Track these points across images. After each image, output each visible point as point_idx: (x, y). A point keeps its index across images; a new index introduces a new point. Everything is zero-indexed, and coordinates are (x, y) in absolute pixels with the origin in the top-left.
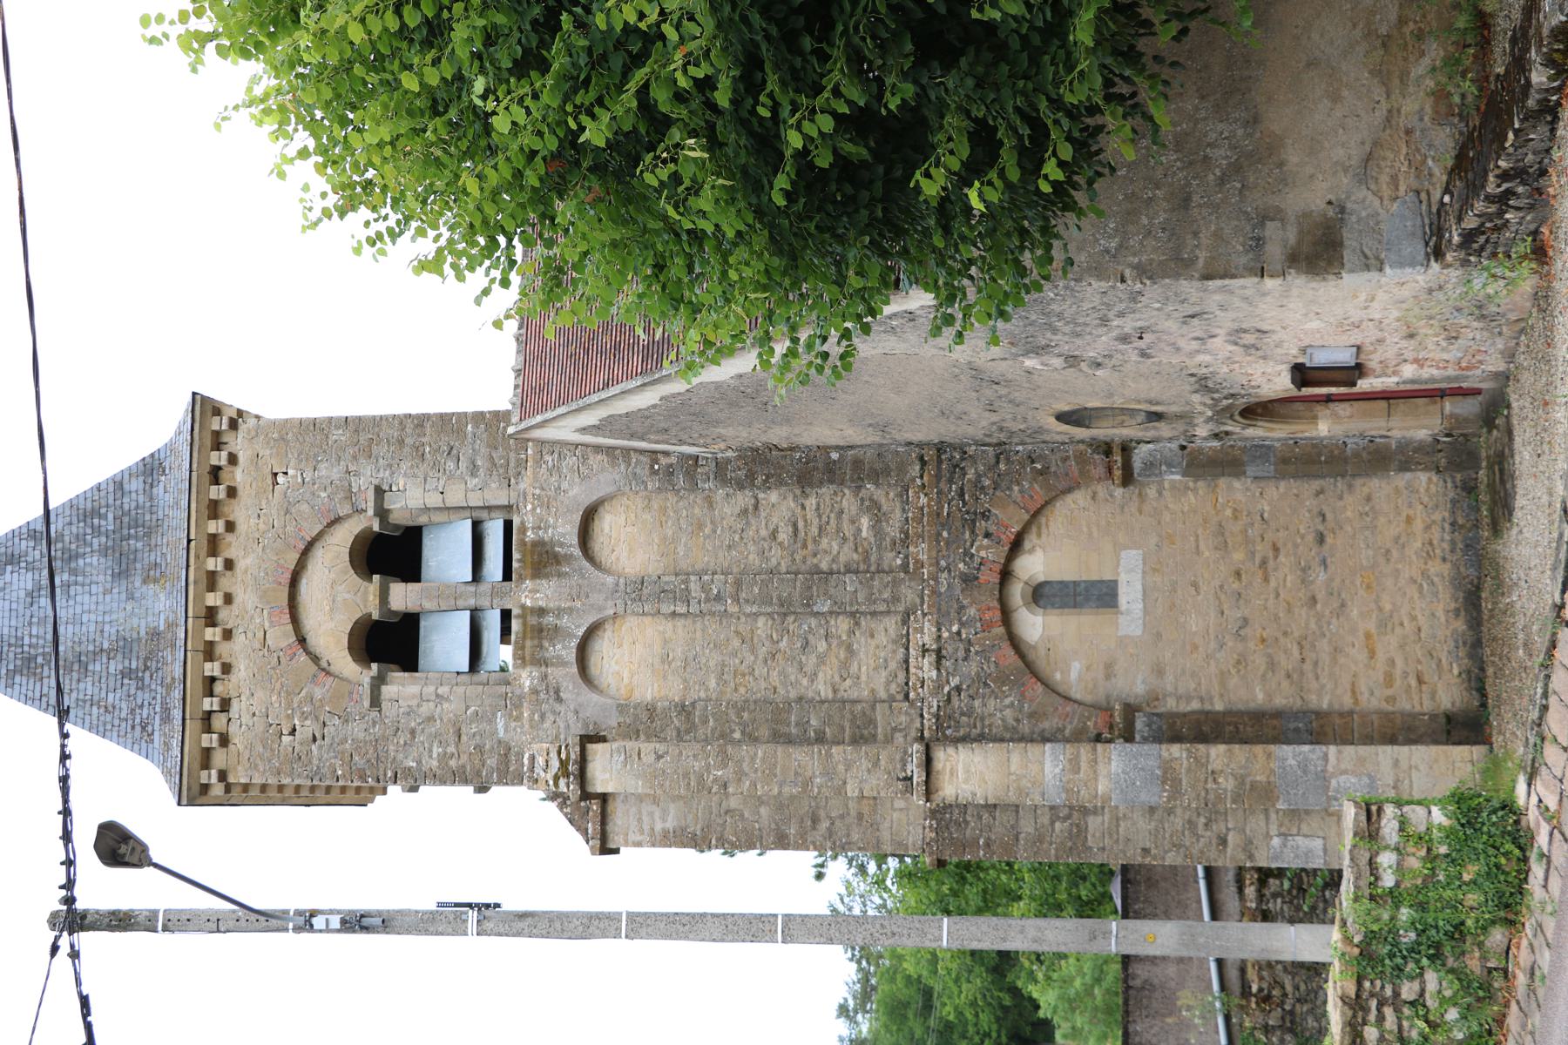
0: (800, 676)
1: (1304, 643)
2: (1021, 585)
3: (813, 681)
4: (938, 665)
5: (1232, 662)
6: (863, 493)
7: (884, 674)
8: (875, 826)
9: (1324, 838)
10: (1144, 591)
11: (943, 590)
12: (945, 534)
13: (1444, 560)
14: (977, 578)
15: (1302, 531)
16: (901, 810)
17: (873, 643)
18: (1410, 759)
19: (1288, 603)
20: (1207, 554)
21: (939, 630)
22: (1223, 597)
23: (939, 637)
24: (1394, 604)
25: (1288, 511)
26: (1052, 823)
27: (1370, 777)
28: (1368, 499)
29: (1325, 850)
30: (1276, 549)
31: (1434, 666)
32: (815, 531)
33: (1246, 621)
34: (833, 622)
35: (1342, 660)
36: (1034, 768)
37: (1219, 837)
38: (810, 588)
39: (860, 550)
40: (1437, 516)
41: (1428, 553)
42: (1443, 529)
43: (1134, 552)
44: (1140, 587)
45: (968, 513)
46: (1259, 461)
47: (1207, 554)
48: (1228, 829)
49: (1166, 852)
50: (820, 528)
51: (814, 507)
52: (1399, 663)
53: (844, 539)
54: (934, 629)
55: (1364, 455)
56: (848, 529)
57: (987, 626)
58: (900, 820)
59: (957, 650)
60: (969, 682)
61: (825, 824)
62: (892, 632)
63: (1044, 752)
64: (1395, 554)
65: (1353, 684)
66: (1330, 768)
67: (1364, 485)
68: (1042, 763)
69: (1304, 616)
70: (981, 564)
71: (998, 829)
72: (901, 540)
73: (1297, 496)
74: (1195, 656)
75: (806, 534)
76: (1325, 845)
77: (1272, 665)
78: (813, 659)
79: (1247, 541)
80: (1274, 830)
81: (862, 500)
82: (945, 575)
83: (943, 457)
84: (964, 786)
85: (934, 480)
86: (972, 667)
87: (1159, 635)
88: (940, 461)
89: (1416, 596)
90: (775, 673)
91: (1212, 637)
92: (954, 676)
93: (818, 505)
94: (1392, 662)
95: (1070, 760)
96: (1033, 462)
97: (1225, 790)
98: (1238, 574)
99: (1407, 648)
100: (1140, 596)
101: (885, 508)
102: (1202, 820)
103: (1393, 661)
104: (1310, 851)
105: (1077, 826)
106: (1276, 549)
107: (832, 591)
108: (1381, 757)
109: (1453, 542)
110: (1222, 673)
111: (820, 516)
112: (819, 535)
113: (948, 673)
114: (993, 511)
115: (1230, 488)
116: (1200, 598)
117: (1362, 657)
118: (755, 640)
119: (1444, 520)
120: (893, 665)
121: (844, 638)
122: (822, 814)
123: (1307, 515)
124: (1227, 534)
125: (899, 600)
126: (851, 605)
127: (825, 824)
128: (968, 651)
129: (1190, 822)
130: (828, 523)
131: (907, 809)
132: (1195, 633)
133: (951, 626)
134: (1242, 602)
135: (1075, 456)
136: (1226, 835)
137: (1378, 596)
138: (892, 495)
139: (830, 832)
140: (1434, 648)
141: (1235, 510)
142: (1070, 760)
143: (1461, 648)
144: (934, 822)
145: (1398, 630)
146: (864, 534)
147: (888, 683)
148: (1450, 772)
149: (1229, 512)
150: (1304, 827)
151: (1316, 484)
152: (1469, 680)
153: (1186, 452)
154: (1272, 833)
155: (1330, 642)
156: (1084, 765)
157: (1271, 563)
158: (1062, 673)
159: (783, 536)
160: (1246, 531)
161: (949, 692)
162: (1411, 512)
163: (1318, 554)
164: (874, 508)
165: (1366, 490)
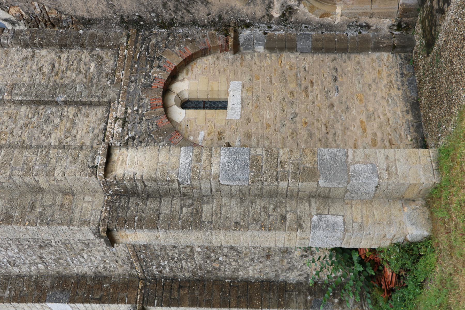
0: (41, 135)
1: (328, 125)
2: (175, 95)
3: (48, 137)
4: (123, 126)
5: (289, 133)
6: (94, 52)
7: (91, 135)
8: (71, 211)
9: (343, 216)
10: (242, 100)
11: (131, 91)
12: (136, 66)
13: (399, 89)
14: (151, 86)
15: (325, 76)
16: (89, 202)
17: (88, 120)
18: (395, 156)
19: (319, 107)
20: (276, 84)
21: (126, 109)
22: (284, 104)
23: (126, 112)
24: (374, 108)
25: (318, 67)
26: (181, 208)
27: (372, 164)
28: (359, 63)
29: (344, 223)
30: (312, 83)
31: (398, 136)
32: (64, 68)
33: (296, 115)
34: (66, 109)
35: (348, 133)
36: (173, 159)
37: (281, 215)
38: (56, 89)
39: (88, 77)
40: (394, 71)
41: (390, 86)
42: (397, 76)
43: (237, 82)
44: (239, 98)
45: (150, 57)
46: (304, 40)
47: (276, 84)
48: (286, 211)
49: (249, 224)
50: (67, 67)
51: (66, 57)
52: (379, 135)
53: (80, 72)
54: (123, 109)
55: (357, 39)
56: (82, 68)
57: (153, 108)
58: (87, 207)
59: (135, 118)
60: (140, 134)
61: (38, 210)
62: (99, 115)
63: (180, 151)
64: (373, 86)
65: (355, 144)
66: (349, 160)
67: (356, 57)
68: (179, 157)
69: (327, 112)
70: (154, 79)
71: (148, 211)
72: (111, 73)
73: (323, 61)
74: (268, 130)
75: (59, 69)
76: (344, 220)
77: (311, 135)
78: (51, 127)
79: (297, 79)
80: (314, 212)
81: (93, 55)
82: (134, 84)
83: (140, 34)
84: (129, 169)
85: (134, 43)
86: (144, 126)
87: (249, 120)
88: (138, 35)
89: (386, 104)
90: (26, 134)
91: (278, 121)
92: (131, 131)
93: (68, 57)
94: (375, 135)
95: (196, 156)
96: (187, 37)
97: (288, 172)
98: (292, 93)
99: (383, 128)
100: (239, 101)
101: (105, 59)
102: (272, 206)
103: (376, 133)
104: (336, 223)
105: (196, 209)
106: (312, 83)
107: (68, 91)
108: (378, 155)
109: (402, 82)
110: (283, 138)
111: (68, 62)
112: (66, 70)
113: (128, 130)
114: (164, 57)
115: (288, 57)
116: (271, 103)
117: (359, 131)
118: (18, 117)
119: (397, 72)
120: (97, 131)
121: (71, 117)
122: (38, 204)
123: (328, 69)
124: (287, 76)
125: (106, 96)
126: (78, 98)
127: (38, 210)
128: (141, 119)
129: (264, 207)
130: (72, 65)
131: (93, 202)
132: (269, 119)
133: (133, 107)
134: (294, 105)
135: (209, 36)
136: (286, 214)
137: (366, 104)
138: (109, 54)
139: (41, 214)
140: (397, 128)
141: (291, 66)
142: (196, 156)
143: (411, 128)
144: (108, 208)
145: (377, 120)
146: (92, 70)
147: (93, 139)
148: (418, 163)
149: (288, 67)
150: (332, 210)
151: (332, 56)
152: (417, 143)
153: (267, 35)
154: (313, 214)
155: (342, 124)
156: (204, 158)
157: (310, 89)
158: (194, 136)
159: (45, 70)
160: (297, 75)
161: (128, 139)
162: (380, 69)
163: (334, 86)
164: (100, 61)
165: (357, 60)
